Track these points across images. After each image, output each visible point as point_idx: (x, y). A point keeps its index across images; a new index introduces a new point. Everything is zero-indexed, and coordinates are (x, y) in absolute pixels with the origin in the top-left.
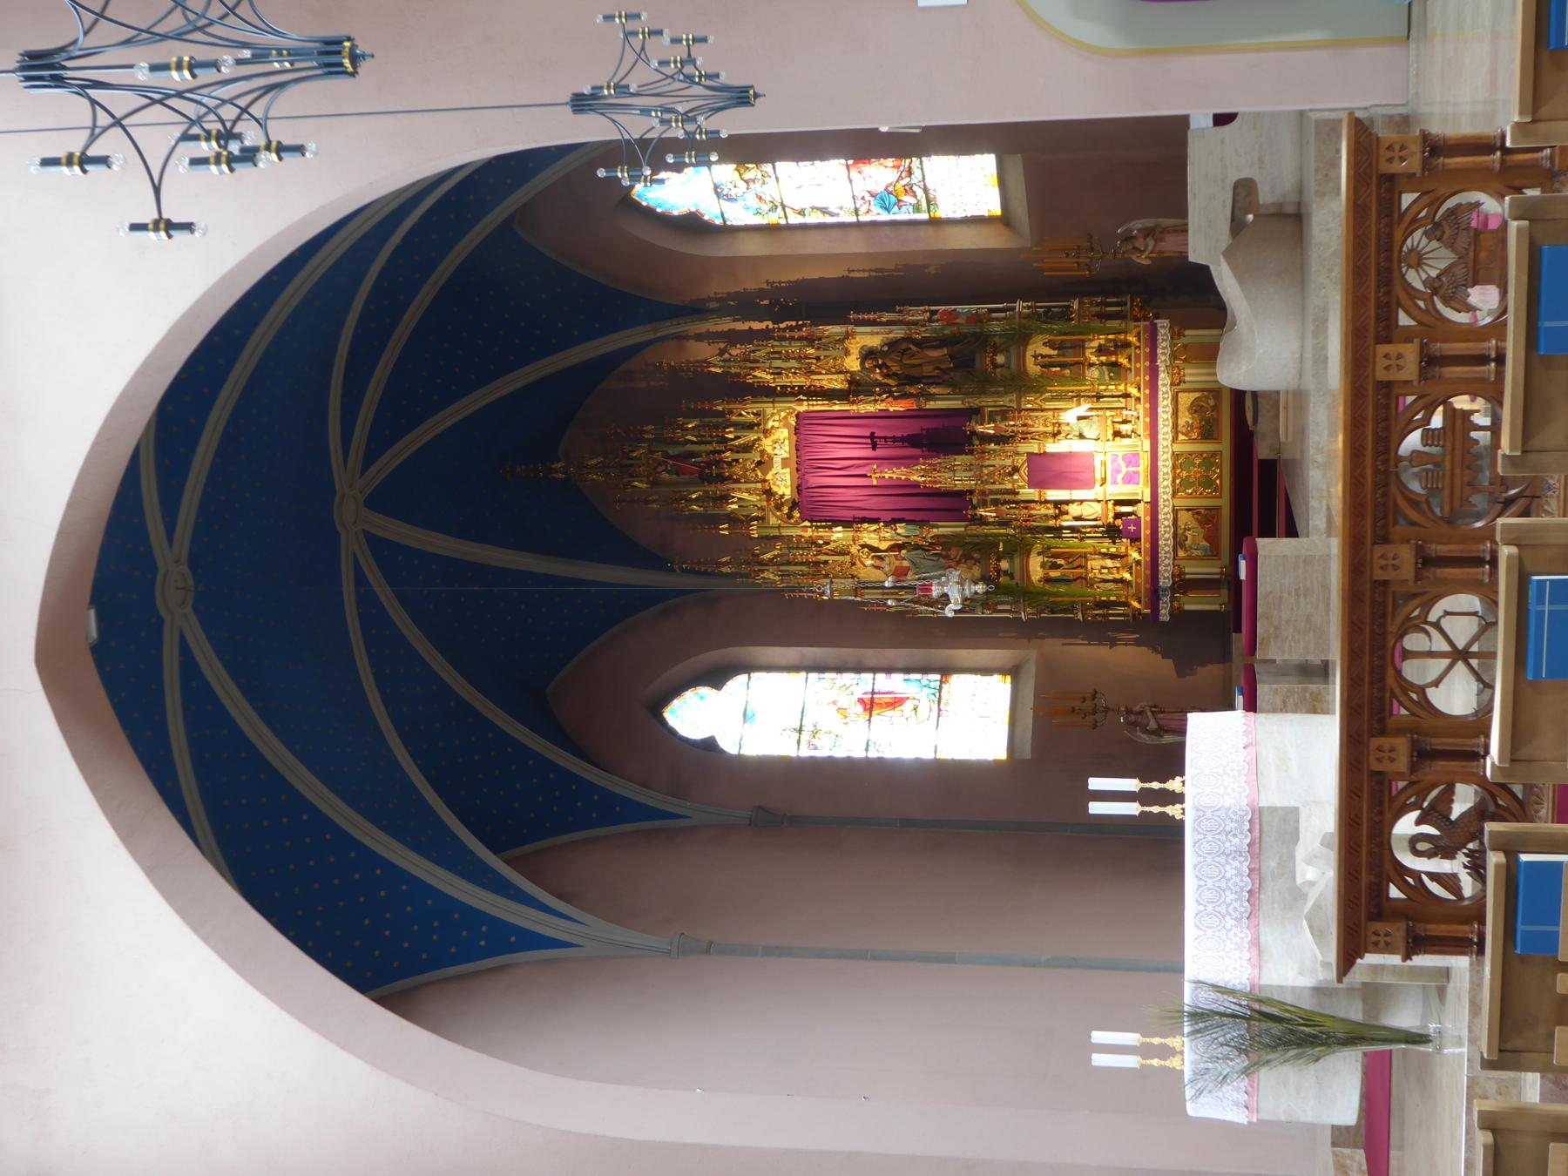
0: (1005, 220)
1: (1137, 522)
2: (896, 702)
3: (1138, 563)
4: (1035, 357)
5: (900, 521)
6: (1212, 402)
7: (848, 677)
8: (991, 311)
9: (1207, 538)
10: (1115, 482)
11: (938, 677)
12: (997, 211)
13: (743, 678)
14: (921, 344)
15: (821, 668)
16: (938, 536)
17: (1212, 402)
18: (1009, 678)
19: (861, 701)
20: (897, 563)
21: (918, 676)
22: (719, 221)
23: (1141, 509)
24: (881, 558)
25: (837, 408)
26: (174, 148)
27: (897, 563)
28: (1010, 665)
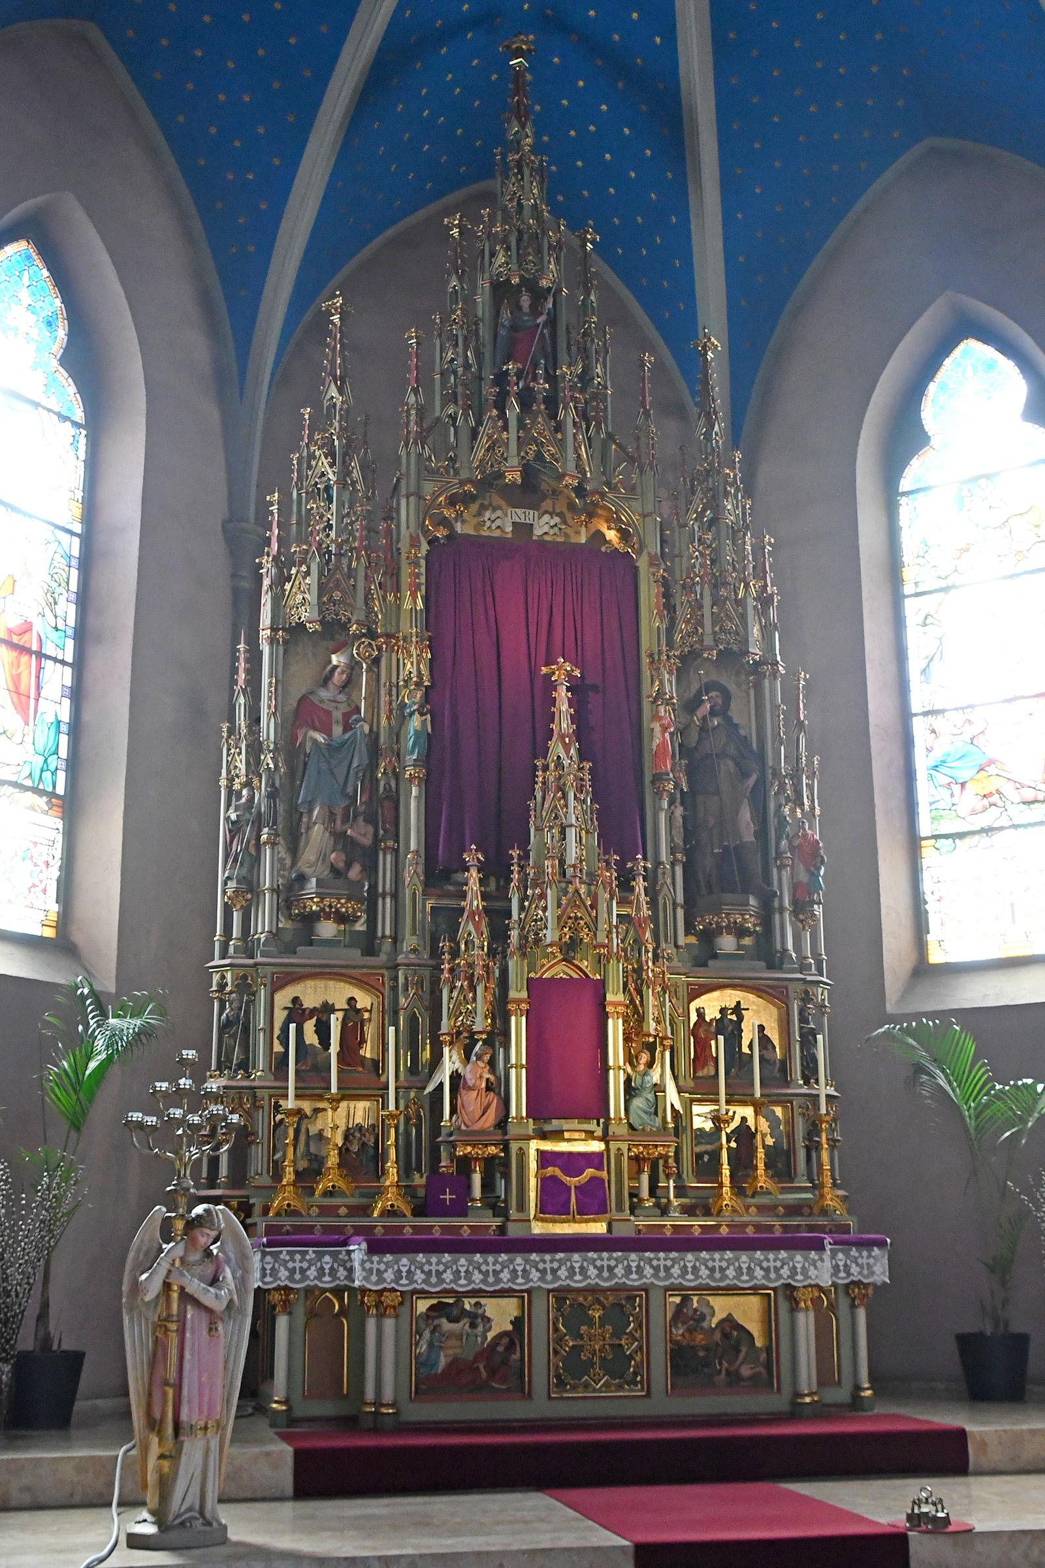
1: (460, 1208)
2: (24, 700)
4: (737, 1009)
6: (746, 1371)
7: (69, 612)
9: (455, 1365)
10: (545, 1158)
12: (936, 956)
13: (79, 415)
14: (759, 799)
15: (89, 561)
18: (49, 933)
19: (27, 628)
20: (337, 715)
21: (63, 752)
22: (905, 484)
26: (1025, 826)
28: (78, 937)
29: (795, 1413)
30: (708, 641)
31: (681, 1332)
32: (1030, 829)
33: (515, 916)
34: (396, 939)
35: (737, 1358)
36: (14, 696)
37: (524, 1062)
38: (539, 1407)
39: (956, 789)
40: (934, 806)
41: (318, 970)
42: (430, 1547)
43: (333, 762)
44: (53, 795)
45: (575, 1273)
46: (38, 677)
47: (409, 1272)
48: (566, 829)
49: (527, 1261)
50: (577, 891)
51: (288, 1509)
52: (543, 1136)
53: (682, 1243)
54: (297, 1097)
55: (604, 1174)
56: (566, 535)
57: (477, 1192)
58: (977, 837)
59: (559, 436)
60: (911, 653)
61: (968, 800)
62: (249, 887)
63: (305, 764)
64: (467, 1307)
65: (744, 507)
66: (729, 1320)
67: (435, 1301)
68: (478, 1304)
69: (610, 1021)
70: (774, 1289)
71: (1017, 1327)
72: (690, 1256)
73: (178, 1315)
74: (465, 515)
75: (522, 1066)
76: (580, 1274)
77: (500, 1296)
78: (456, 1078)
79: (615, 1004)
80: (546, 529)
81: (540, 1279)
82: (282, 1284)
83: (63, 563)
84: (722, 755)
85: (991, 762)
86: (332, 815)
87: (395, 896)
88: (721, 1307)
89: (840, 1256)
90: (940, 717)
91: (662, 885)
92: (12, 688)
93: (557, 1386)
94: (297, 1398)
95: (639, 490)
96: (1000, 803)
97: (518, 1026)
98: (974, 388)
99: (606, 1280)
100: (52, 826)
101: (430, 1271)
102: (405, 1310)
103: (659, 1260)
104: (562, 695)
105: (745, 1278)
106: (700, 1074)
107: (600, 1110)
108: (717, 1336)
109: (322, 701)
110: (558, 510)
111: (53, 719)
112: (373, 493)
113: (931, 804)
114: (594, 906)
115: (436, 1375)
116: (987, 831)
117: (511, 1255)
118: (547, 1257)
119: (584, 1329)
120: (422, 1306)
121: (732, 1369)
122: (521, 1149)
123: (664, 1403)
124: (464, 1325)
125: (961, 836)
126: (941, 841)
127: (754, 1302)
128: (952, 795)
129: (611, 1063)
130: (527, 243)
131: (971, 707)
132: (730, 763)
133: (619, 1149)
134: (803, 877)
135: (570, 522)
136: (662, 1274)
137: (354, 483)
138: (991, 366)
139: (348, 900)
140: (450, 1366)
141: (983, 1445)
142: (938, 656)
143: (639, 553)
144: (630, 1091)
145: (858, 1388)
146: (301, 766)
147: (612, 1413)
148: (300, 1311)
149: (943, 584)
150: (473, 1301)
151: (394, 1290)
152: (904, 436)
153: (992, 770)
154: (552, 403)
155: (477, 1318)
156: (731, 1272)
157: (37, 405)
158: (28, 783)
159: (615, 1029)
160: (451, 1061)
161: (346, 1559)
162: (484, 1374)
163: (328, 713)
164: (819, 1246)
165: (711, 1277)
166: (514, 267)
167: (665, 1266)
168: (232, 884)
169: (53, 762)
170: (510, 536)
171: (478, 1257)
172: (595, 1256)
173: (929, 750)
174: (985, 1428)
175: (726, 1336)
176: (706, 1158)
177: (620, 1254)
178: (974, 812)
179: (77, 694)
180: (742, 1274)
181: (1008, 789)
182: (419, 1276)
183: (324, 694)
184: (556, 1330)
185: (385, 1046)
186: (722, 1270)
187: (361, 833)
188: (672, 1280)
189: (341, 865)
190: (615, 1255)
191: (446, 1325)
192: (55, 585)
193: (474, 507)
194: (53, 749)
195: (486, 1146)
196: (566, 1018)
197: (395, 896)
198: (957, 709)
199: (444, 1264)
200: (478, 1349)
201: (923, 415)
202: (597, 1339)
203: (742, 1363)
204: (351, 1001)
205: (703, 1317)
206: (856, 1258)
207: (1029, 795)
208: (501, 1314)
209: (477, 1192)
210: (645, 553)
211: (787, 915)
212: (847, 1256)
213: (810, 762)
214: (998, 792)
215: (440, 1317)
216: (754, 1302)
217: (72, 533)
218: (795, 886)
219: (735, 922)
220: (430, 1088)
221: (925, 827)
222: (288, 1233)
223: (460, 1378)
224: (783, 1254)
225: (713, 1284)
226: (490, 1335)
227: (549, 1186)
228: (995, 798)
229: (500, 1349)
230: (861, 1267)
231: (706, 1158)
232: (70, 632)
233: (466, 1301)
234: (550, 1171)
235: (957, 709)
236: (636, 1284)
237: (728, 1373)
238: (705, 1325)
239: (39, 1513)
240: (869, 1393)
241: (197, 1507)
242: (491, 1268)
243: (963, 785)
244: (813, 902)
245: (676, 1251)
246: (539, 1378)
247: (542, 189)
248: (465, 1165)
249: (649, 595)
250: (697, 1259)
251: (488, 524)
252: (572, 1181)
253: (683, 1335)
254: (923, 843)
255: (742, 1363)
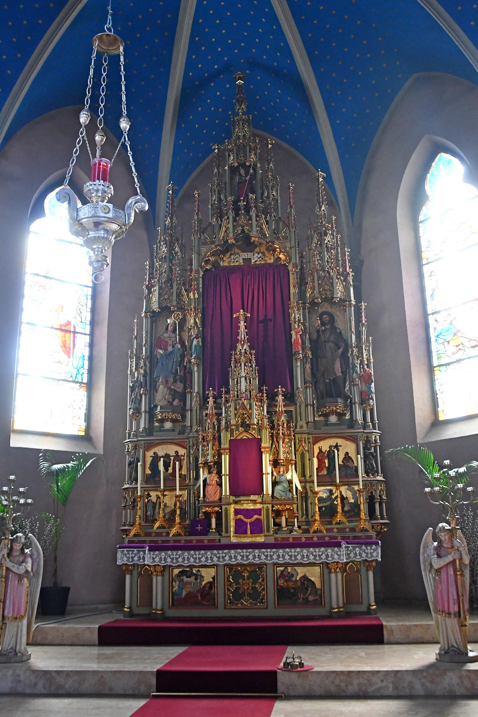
0: (436, 424)
2: (67, 349)
3: (168, 534)
4: (337, 447)
5: (203, 341)
6: (311, 598)
8: (372, 411)
9: (189, 595)
10: (237, 512)
11: (85, 381)
12: (442, 418)
14: (344, 358)
15: (95, 297)
16: (191, 373)
17: (311, 598)
18: (83, 434)
19: (69, 323)
20: (170, 342)
22: (421, 218)
23: (213, 536)
24: (174, 331)
25: (292, 290)
27: (170, 342)
28: (92, 434)
29: (330, 616)
30: (317, 295)
31: (282, 582)
32: (475, 358)
33: (224, 415)
34: (191, 427)
35: (307, 593)
36: (64, 348)
37: (228, 473)
38: (221, 612)
39: (446, 344)
40: (438, 353)
41: (161, 441)
42: (92, 668)
43: (168, 361)
44: (82, 383)
45: (357, 555)
46: (74, 341)
47: (165, 558)
48: (244, 377)
49: (212, 554)
50: (243, 403)
51: (95, 651)
52: (236, 502)
53: (297, 544)
54: (180, 489)
55: (262, 517)
56: (265, 260)
57: (214, 525)
58: (455, 364)
59: (250, 222)
60: (427, 289)
61: (451, 348)
62: (137, 411)
63: (157, 362)
64: (194, 572)
65: (337, 238)
66: (305, 578)
67: (181, 570)
68: (199, 571)
69: (263, 455)
70: (360, 562)
71: (64, 584)
72: (281, 551)
73: (5, 575)
74: (225, 258)
75: (227, 475)
76: (282, 558)
77: (208, 567)
78: (205, 481)
79: (265, 448)
80: (256, 259)
81: (217, 561)
82: (336, 561)
83: (84, 298)
84: (329, 341)
85: (459, 331)
86: (167, 382)
87: (191, 411)
88: (301, 572)
89: (357, 549)
90: (438, 314)
91: (298, 397)
92: (62, 345)
93: (230, 603)
94: (134, 606)
95: (289, 238)
96: (463, 349)
97: (226, 460)
98: (447, 173)
99: (244, 561)
100: (83, 394)
101: (196, 558)
102: (166, 573)
103: (243, 552)
104: (242, 324)
105: (305, 559)
106: (320, 474)
107: (260, 491)
108: (299, 583)
109: (165, 338)
110: (262, 251)
111: (81, 355)
112: (185, 256)
113: (437, 352)
114: (250, 409)
115: (181, 598)
116: (458, 361)
117: (326, 548)
118: (221, 552)
119: (240, 581)
120: (176, 571)
121: (305, 597)
122: (226, 508)
123: (272, 611)
124: (192, 579)
125: (449, 364)
126: (442, 367)
127: (317, 569)
128: (445, 347)
129: (264, 472)
130: (241, 150)
131: (450, 308)
132: (332, 345)
133: (267, 507)
134: (364, 388)
135: (267, 255)
136: (269, 558)
137: (176, 253)
138: (449, 162)
139: (173, 414)
140: (187, 595)
141: (392, 631)
142: (436, 290)
143: (289, 263)
144: (275, 483)
145: (370, 605)
146: (155, 363)
147: (281, 615)
148: (135, 573)
149: (437, 257)
150: (197, 569)
151: (158, 565)
152: (418, 198)
153: (459, 334)
154: (248, 209)
155: (198, 577)
156: (299, 557)
157: (71, 243)
158: (71, 379)
159: (266, 458)
160: (203, 475)
161: (43, 671)
162: (200, 599)
163: (166, 342)
164: (339, 545)
165: (290, 559)
166: (235, 160)
167: (270, 555)
168: (132, 410)
169: (81, 371)
170: (242, 264)
171: (192, 552)
172: (265, 551)
173: (435, 329)
174: (391, 623)
175: (302, 583)
176: (324, 509)
177: (227, 551)
178: (453, 354)
179: (91, 345)
180: (357, 555)
181: (465, 342)
182: (169, 560)
183: (166, 335)
184: (229, 581)
185: (181, 470)
186: (295, 556)
187: (179, 387)
188: (298, 561)
189: (171, 400)
190: (249, 550)
191: (185, 579)
192: (81, 306)
193: (228, 255)
194: (81, 366)
195: (214, 507)
196: (246, 455)
197: (191, 411)
198: (444, 310)
199: (350, 551)
200: (198, 588)
201: (426, 188)
202: (247, 585)
203: (309, 595)
204: (177, 452)
205: (293, 576)
206: (365, 550)
207: (474, 343)
208: (208, 575)
209: (214, 525)
210: (291, 263)
211: (357, 405)
212: (360, 549)
213: (368, 340)
214: (462, 344)
215: (182, 576)
216: (317, 569)
217: (88, 287)
218: (361, 393)
219: (333, 410)
220: (198, 485)
221: (435, 363)
222: (136, 543)
223: (191, 600)
224: (323, 549)
225: (291, 562)
226: (204, 583)
227: (238, 522)
228: (461, 347)
229: (207, 588)
230: (367, 554)
231: (324, 509)
232: (88, 323)
233: (194, 569)
234: (239, 516)
235: (444, 310)
236: (235, 563)
237: (303, 599)
238: (294, 579)
239: (412, 648)
240: (375, 607)
241: (14, 648)
242: (197, 556)
243: (448, 342)
244: (369, 399)
245: (275, 548)
246: (220, 600)
247: (249, 128)
248: (208, 515)
249: (293, 279)
250: (284, 552)
251: (233, 260)
252: (248, 521)
253: (283, 583)
254: (435, 369)
255: (309, 595)
